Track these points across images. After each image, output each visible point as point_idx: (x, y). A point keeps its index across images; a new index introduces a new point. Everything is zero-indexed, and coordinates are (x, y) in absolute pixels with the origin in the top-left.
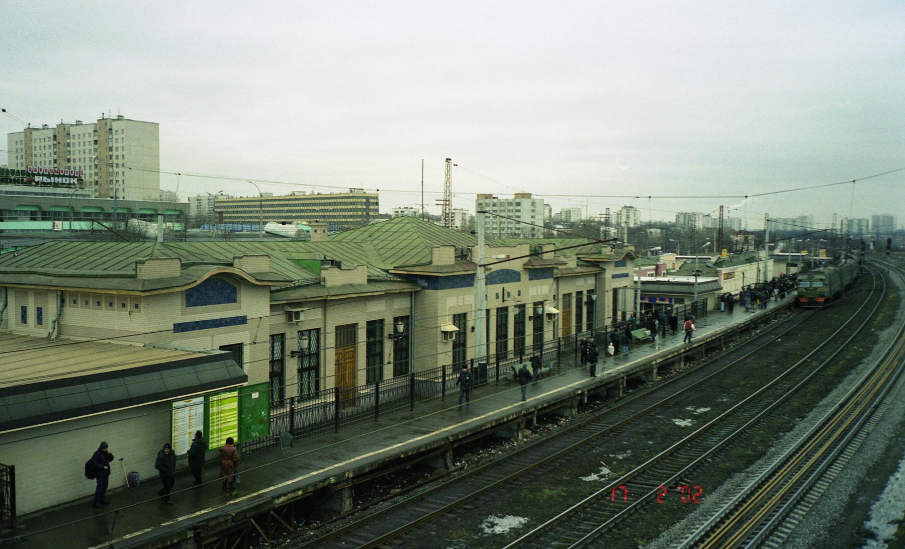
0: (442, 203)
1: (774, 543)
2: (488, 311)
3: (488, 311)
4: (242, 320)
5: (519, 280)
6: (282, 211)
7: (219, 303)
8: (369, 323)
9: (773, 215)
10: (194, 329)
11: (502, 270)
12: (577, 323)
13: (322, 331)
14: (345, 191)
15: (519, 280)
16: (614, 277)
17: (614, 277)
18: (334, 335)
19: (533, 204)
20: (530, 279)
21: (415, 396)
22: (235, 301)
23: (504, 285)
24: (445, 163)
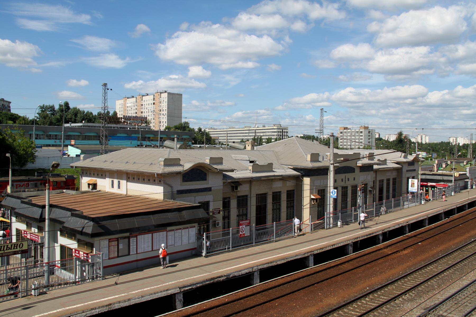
0: (319, 131)
1: (354, 311)
2: (472, 188)
3: (472, 188)
4: (209, 189)
5: (354, 172)
6: (243, 133)
7: (198, 181)
8: (273, 193)
9: (404, 134)
10: (186, 193)
11: (345, 167)
12: (387, 193)
13: (249, 196)
14: (440, 142)
15: (354, 172)
16: (407, 171)
17: (407, 171)
18: (255, 198)
19: (369, 132)
20: (360, 172)
21: (117, 240)
22: (206, 180)
23: (346, 174)
24: (320, 111)
